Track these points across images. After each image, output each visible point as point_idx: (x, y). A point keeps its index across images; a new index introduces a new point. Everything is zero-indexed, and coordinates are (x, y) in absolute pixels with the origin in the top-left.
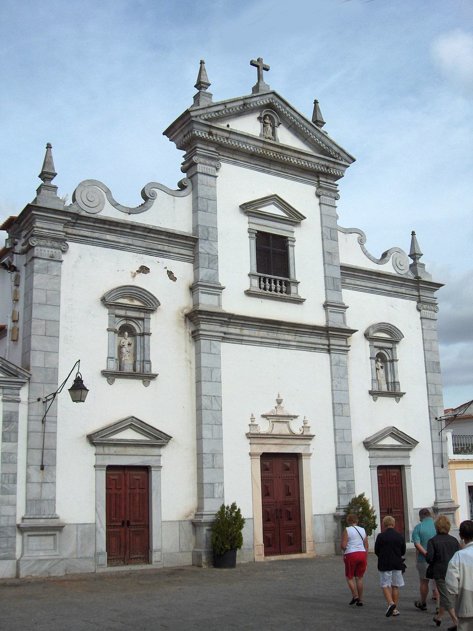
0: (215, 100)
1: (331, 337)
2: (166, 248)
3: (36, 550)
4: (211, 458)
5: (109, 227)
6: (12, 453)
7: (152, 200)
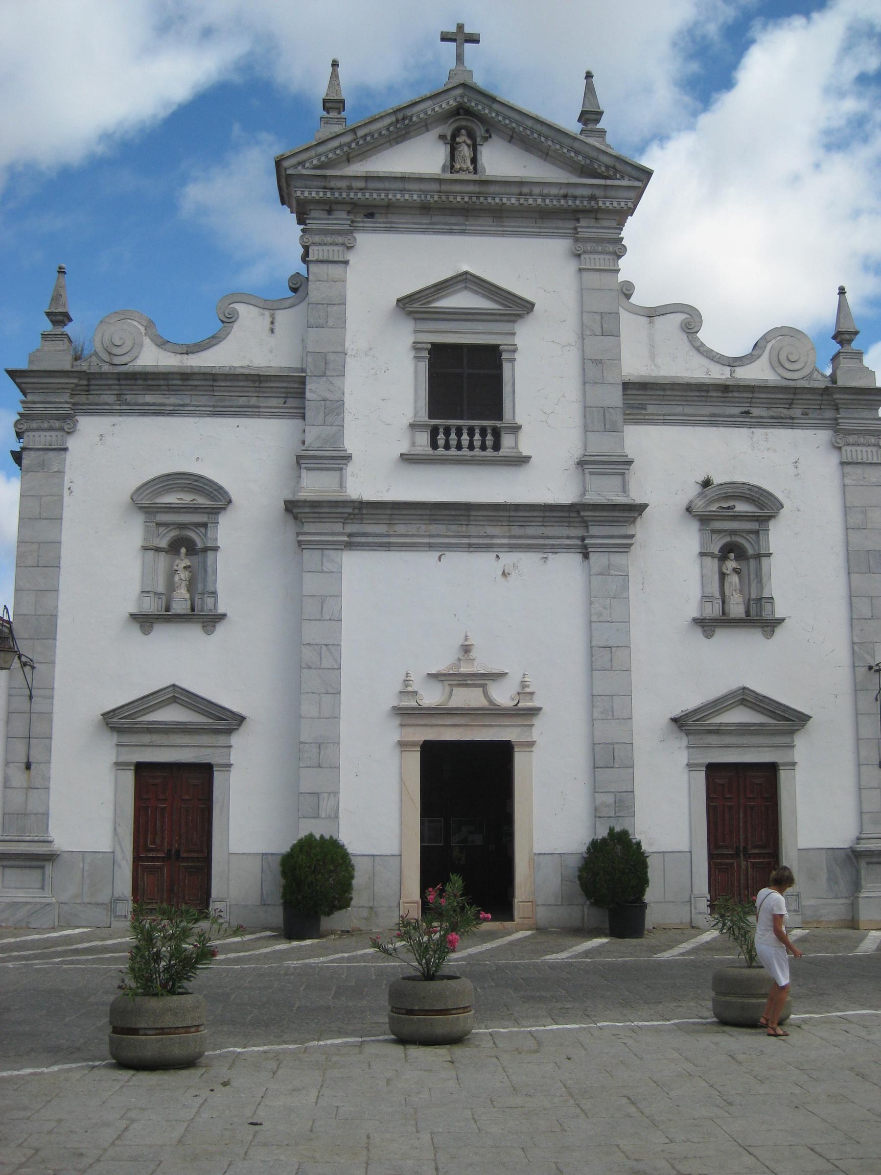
2: (253, 401)
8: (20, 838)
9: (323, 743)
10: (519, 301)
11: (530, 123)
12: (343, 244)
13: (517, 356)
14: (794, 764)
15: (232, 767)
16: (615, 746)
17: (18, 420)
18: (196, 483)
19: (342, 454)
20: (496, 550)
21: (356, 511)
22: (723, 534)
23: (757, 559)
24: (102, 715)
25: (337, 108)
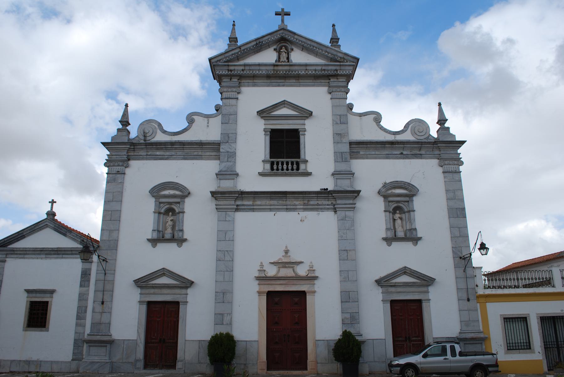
1: (337, 198)
2: (200, 153)
3: (94, 356)
4: (222, 295)
5: (156, 147)
6: (85, 294)
7: (192, 124)
8: (97, 334)
9: (225, 292)
10: (306, 111)
11: (309, 42)
15: (188, 303)
16: (350, 292)
17: (106, 162)
18: (175, 186)
20: (298, 211)
21: (240, 196)
24: (134, 281)
25: (234, 41)
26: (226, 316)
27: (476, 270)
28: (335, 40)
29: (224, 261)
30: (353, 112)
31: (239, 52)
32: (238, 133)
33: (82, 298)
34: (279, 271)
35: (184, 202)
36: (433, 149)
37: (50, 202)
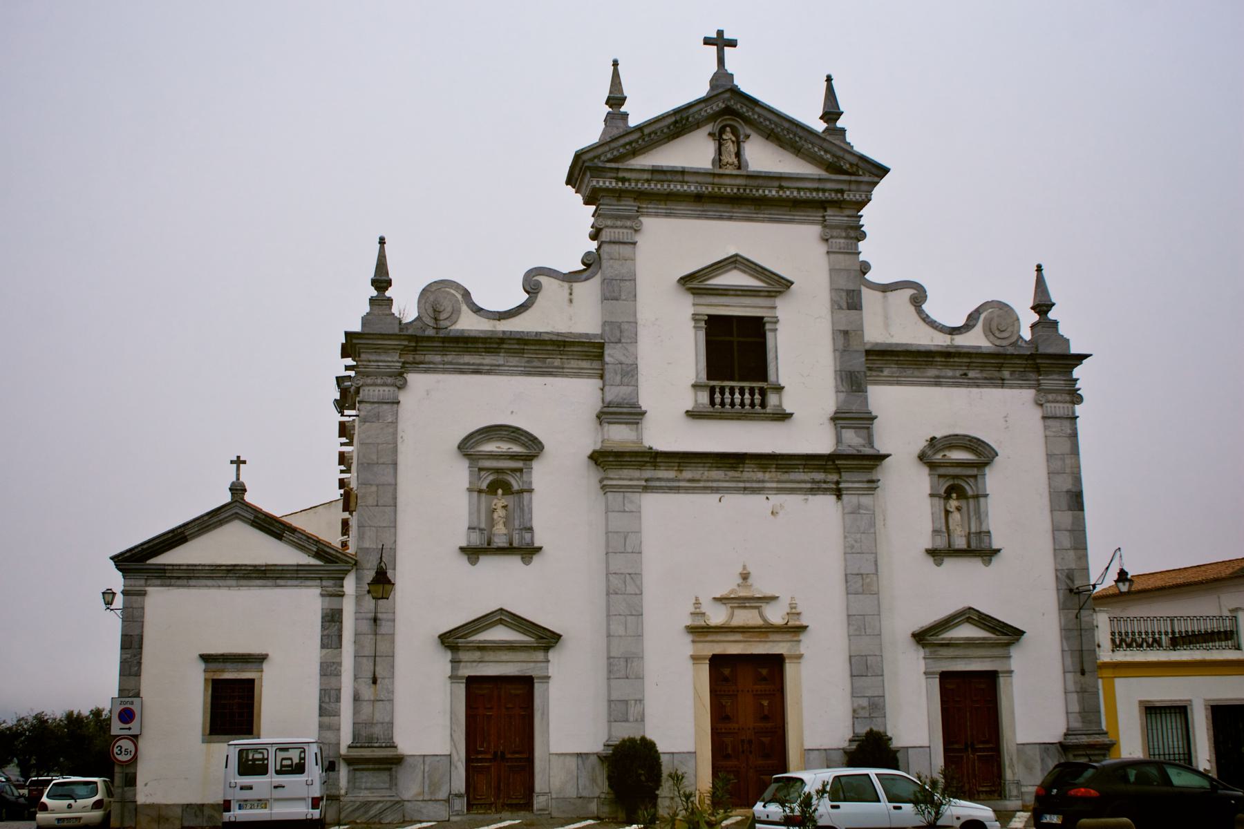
0: (633, 122)
12: (631, 228)
13: (778, 326)
14: (1011, 672)
16: (868, 657)
19: (638, 410)
20: (767, 492)
22: (948, 478)
23: (976, 500)
26: (633, 705)
27: (1098, 614)
28: (831, 113)
29: (625, 594)
30: (865, 278)
31: (639, 138)
32: (640, 322)
33: (329, 670)
34: (732, 615)
35: (532, 468)
36: (1025, 368)
37: (232, 462)
